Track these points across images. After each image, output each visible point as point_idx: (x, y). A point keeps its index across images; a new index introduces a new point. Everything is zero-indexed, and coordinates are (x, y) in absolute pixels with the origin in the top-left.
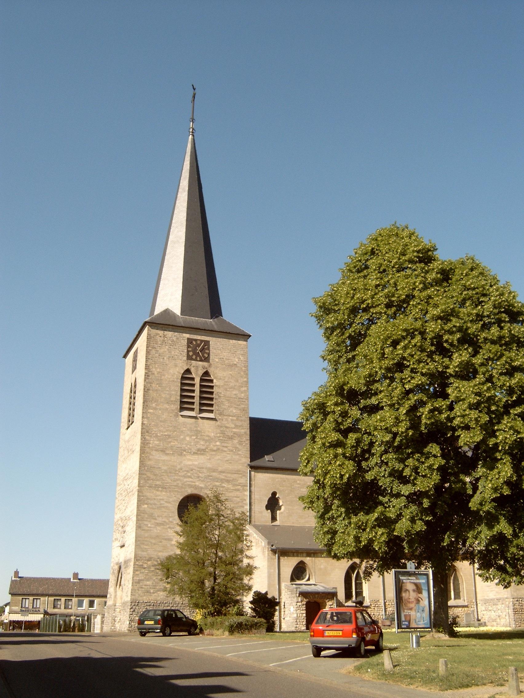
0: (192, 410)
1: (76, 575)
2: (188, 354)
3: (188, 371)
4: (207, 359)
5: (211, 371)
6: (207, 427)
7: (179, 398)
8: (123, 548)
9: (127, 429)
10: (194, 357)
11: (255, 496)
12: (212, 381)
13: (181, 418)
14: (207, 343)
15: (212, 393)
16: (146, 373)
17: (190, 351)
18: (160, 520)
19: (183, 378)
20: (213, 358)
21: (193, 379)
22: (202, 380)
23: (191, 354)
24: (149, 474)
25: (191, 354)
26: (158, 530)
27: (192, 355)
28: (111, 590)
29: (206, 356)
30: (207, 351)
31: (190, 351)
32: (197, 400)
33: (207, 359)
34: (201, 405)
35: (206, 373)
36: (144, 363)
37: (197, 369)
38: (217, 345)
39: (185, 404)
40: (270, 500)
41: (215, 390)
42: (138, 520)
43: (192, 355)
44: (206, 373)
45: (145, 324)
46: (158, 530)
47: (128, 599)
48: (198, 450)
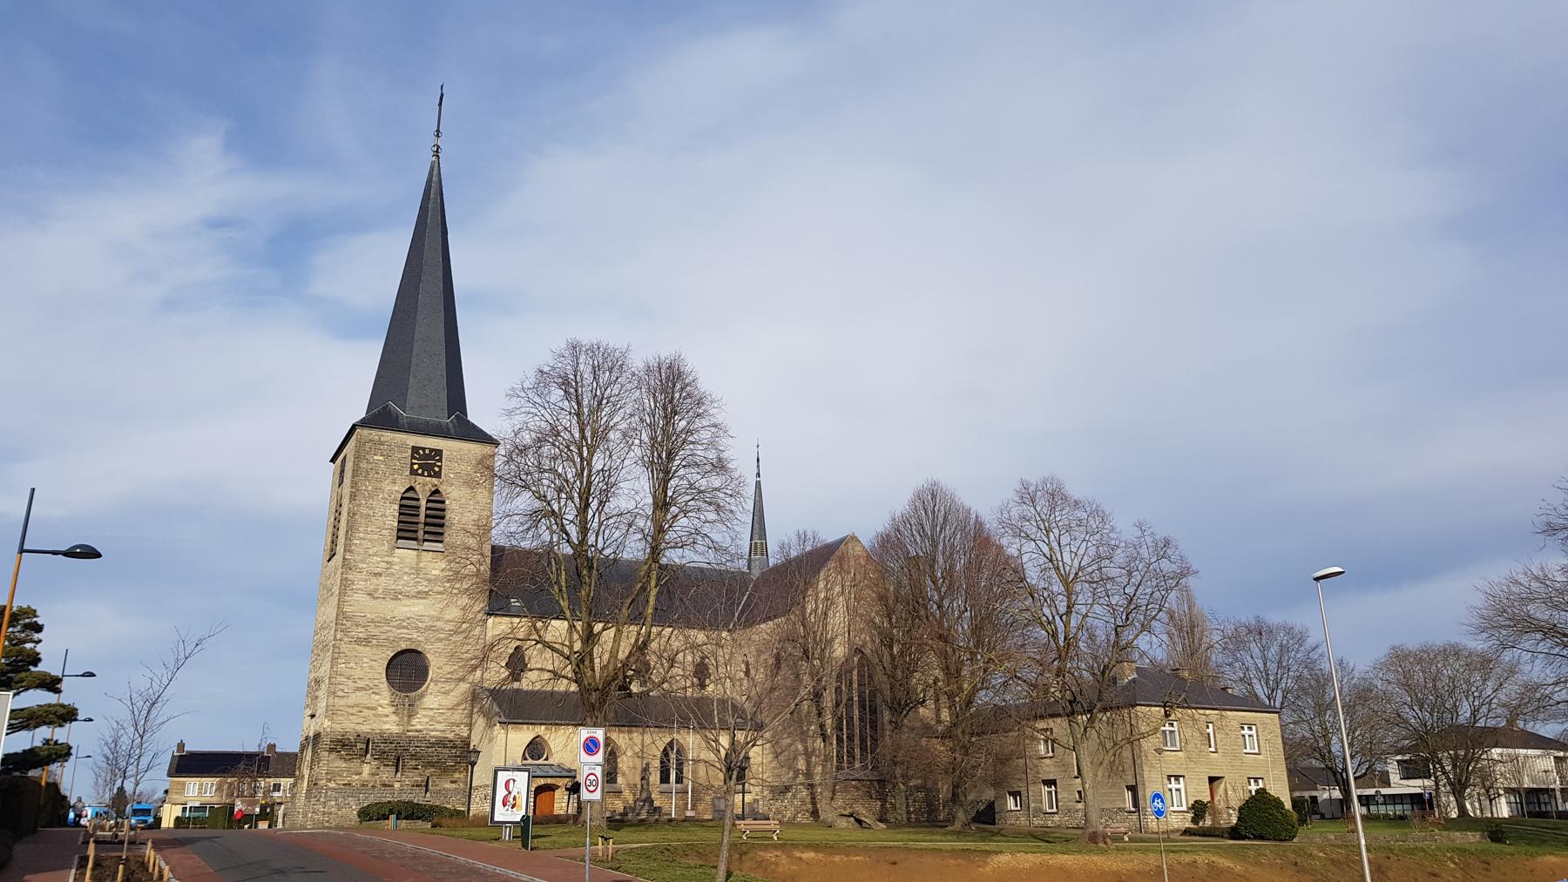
3: (411, 489)
14: (439, 452)
18: (361, 684)
26: (355, 698)
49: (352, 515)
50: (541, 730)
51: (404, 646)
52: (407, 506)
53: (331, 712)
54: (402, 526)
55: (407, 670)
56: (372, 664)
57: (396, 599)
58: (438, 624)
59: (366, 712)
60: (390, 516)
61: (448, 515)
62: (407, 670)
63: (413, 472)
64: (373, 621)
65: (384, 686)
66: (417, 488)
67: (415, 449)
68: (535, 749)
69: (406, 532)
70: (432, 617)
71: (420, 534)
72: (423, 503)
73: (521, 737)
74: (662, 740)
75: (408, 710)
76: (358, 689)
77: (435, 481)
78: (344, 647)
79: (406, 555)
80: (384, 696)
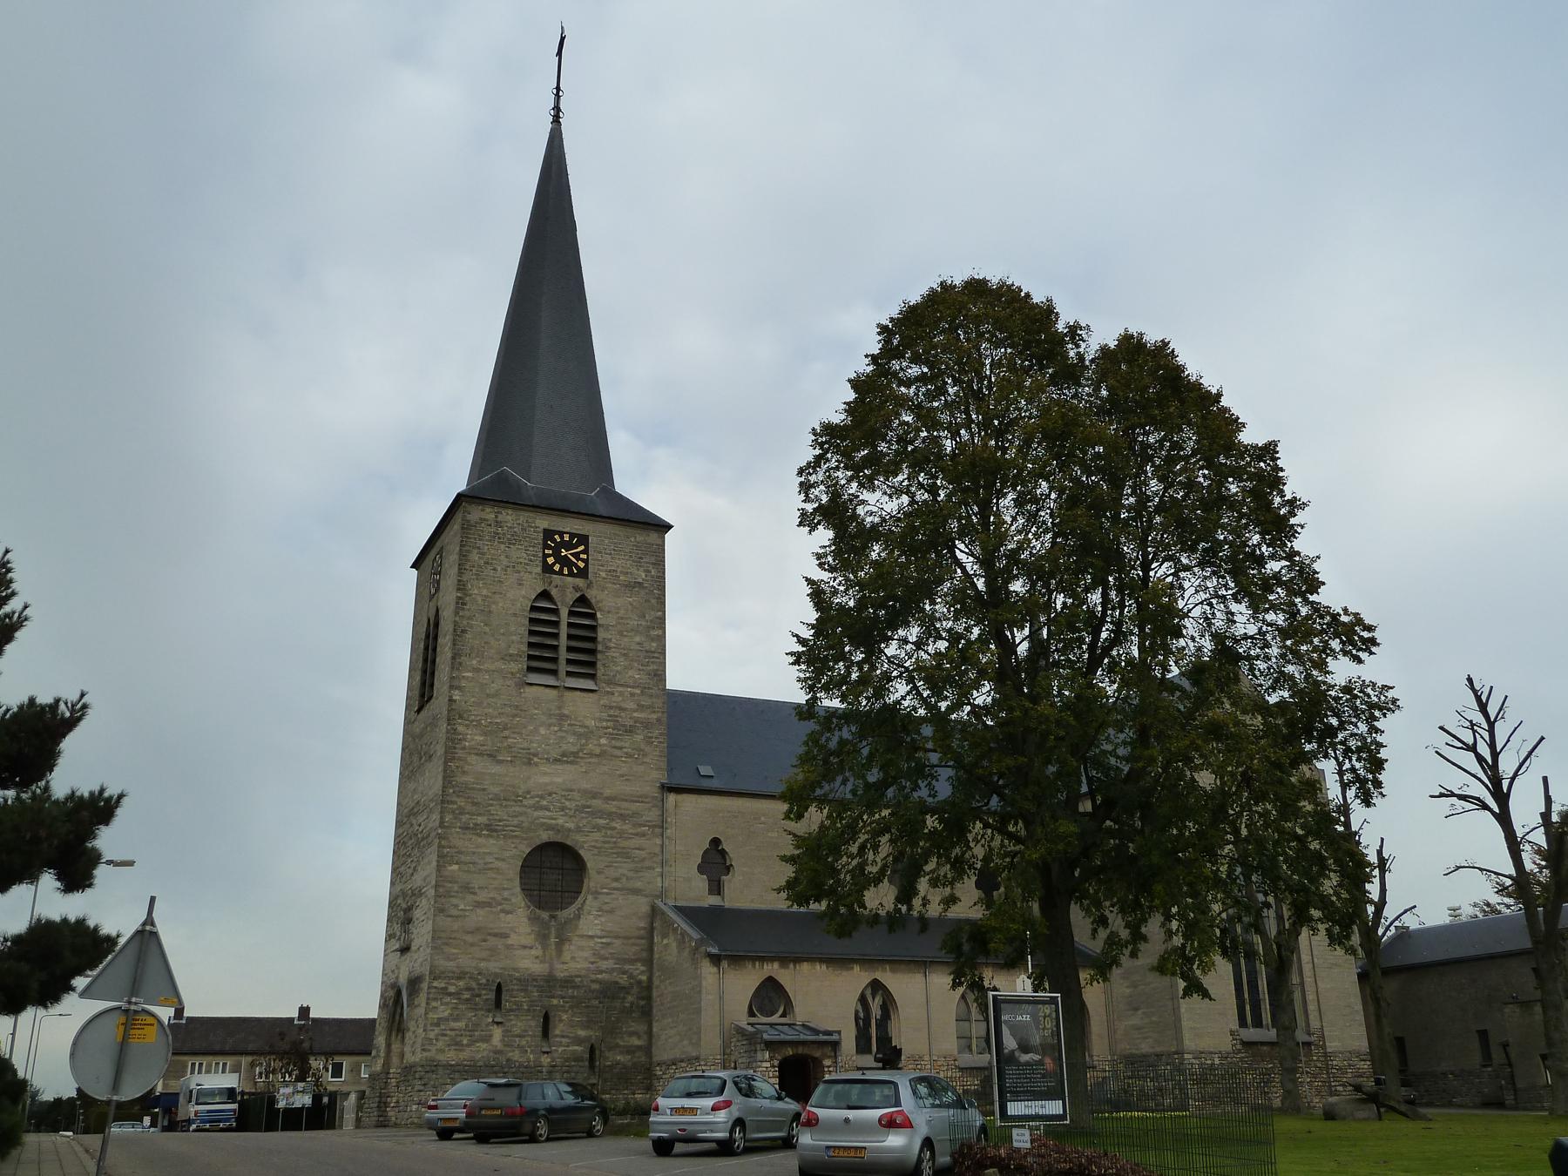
0: (554, 673)
2: (545, 562)
3: (545, 595)
4: (583, 573)
5: (592, 594)
6: (584, 707)
14: (583, 540)
18: (483, 896)
21: (555, 612)
25: (551, 560)
26: (479, 917)
33: (583, 573)
37: (565, 590)
44: (583, 600)
49: (459, 632)
50: (772, 969)
51: (545, 836)
52: (542, 610)
53: (440, 939)
54: (534, 640)
55: (554, 872)
56: (501, 860)
57: (529, 763)
58: (597, 803)
59: (492, 941)
60: (517, 637)
61: (601, 635)
62: (554, 872)
63: (547, 569)
64: (497, 798)
65: (519, 899)
66: (554, 592)
67: (549, 534)
68: (770, 996)
69: (541, 658)
70: (584, 792)
71: (563, 667)
72: (564, 613)
73: (743, 984)
74: (856, 980)
75: (554, 935)
76: (479, 905)
77: (580, 582)
78: (459, 840)
79: (540, 695)
80: (518, 921)
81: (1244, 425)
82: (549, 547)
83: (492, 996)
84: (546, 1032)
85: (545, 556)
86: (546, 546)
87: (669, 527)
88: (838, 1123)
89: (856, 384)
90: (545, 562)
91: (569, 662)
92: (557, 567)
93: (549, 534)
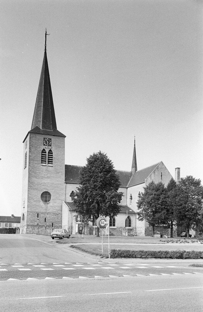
0: (46, 163)
1: (13, 215)
2: (44, 144)
3: (44, 150)
4: (51, 145)
5: (52, 150)
7: (41, 159)
8: (24, 208)
9: (25, 168)
10: (46, 145)
11: (67, 192)
12: (52, 153)
13: (42, 166)
14: (51, 139)
15: (52, 156)
16: (29, 151)
17: (45, 142)
18: (35, 200)
19: (42, 152)
20: (112, 259)
22: (49, 153)
23: (45, 143)
24: (31, 185)
25: (45, 143)
26: (34, 203)
27: (45, 144)
28: (21, 220)
29: (50, 144)
30: (50, 142)
31: (45, 142)
32: (47, 160)
34: (48, 161)
35: (50, 150)
36: (29, 147)
38: (54, 139)
39: (43, 161)
40: (71, 194)
41: (54, 156)
42: (28, 200)
43: (45, 144)
44: (50, 150)
45: (29, 132)
46: (34, 203)
47: (26, 224)
48: (47, 177)
51: (45, 191)
81: (162, 163)
82: (44, 141)
83: (37, 215)
84: (131, 196)
85: (44, 142)
86: (44, 141)
87: (66, 137)
88: (74, 311)
89: (121, 199)
90: (44, 144)
91: (46, 159)
92: (46, 145)
93: (44, 139)
